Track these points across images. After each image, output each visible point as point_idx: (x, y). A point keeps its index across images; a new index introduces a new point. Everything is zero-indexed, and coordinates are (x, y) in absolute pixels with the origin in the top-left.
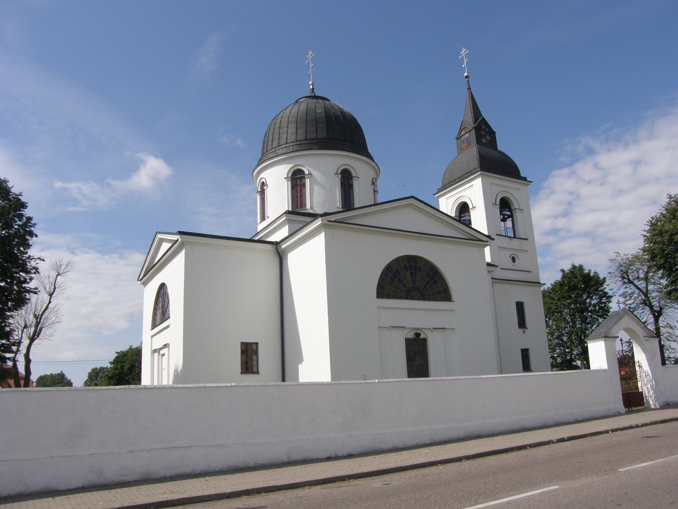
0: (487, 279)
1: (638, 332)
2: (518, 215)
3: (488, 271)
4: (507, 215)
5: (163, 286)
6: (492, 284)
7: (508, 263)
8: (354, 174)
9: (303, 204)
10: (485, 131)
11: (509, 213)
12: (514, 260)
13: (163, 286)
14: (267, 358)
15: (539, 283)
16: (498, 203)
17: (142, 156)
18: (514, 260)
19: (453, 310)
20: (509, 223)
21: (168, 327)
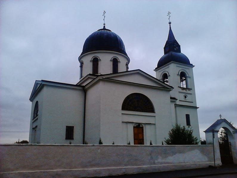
0: (173, 105)
1: (228, 128)
2: (188, 79)
3: (171, 101)
4: (183, 79)
5: (37, 102)
6: (175, 107)
7: (182, 98)
8: (99, 59)
9: (97, 72)
10: (176, 45)
11: (185, 78)
12: (185, 97)
13: (37, 102)
14: (77, 134)
15: (196, 107)
16: (180, 74)
17: (166, 55)
18: (185, 97)
19: (155, 116)
20: (184, 82)
21: (37, 119)
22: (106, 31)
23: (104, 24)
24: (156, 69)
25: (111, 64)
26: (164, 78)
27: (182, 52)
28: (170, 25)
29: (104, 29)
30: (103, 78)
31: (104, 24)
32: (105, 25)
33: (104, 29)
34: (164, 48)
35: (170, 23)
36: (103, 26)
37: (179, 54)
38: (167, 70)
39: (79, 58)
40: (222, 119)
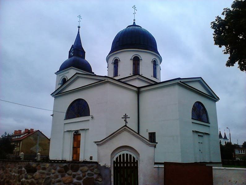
22: (137, 27)
23: (134, 20)
24: (58, 72)
25: (131, 63)
26: (63, 83)
27: (85, 59)
28: (79, 29)
29: (134, 25)
30: (180, 82)
31: (134, 20)
32: (135, 21)
33: (134, 25)
34: (85, 52)
35: (79, 27)
36: (133, 21)
37: (81, 59)
38: (67, 75)
39: (108, 57)
40: (83, 156)
